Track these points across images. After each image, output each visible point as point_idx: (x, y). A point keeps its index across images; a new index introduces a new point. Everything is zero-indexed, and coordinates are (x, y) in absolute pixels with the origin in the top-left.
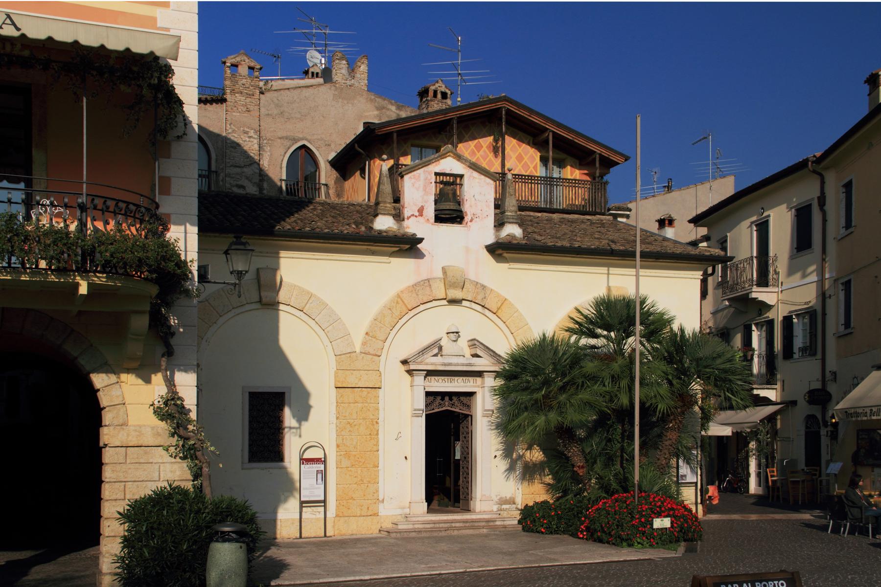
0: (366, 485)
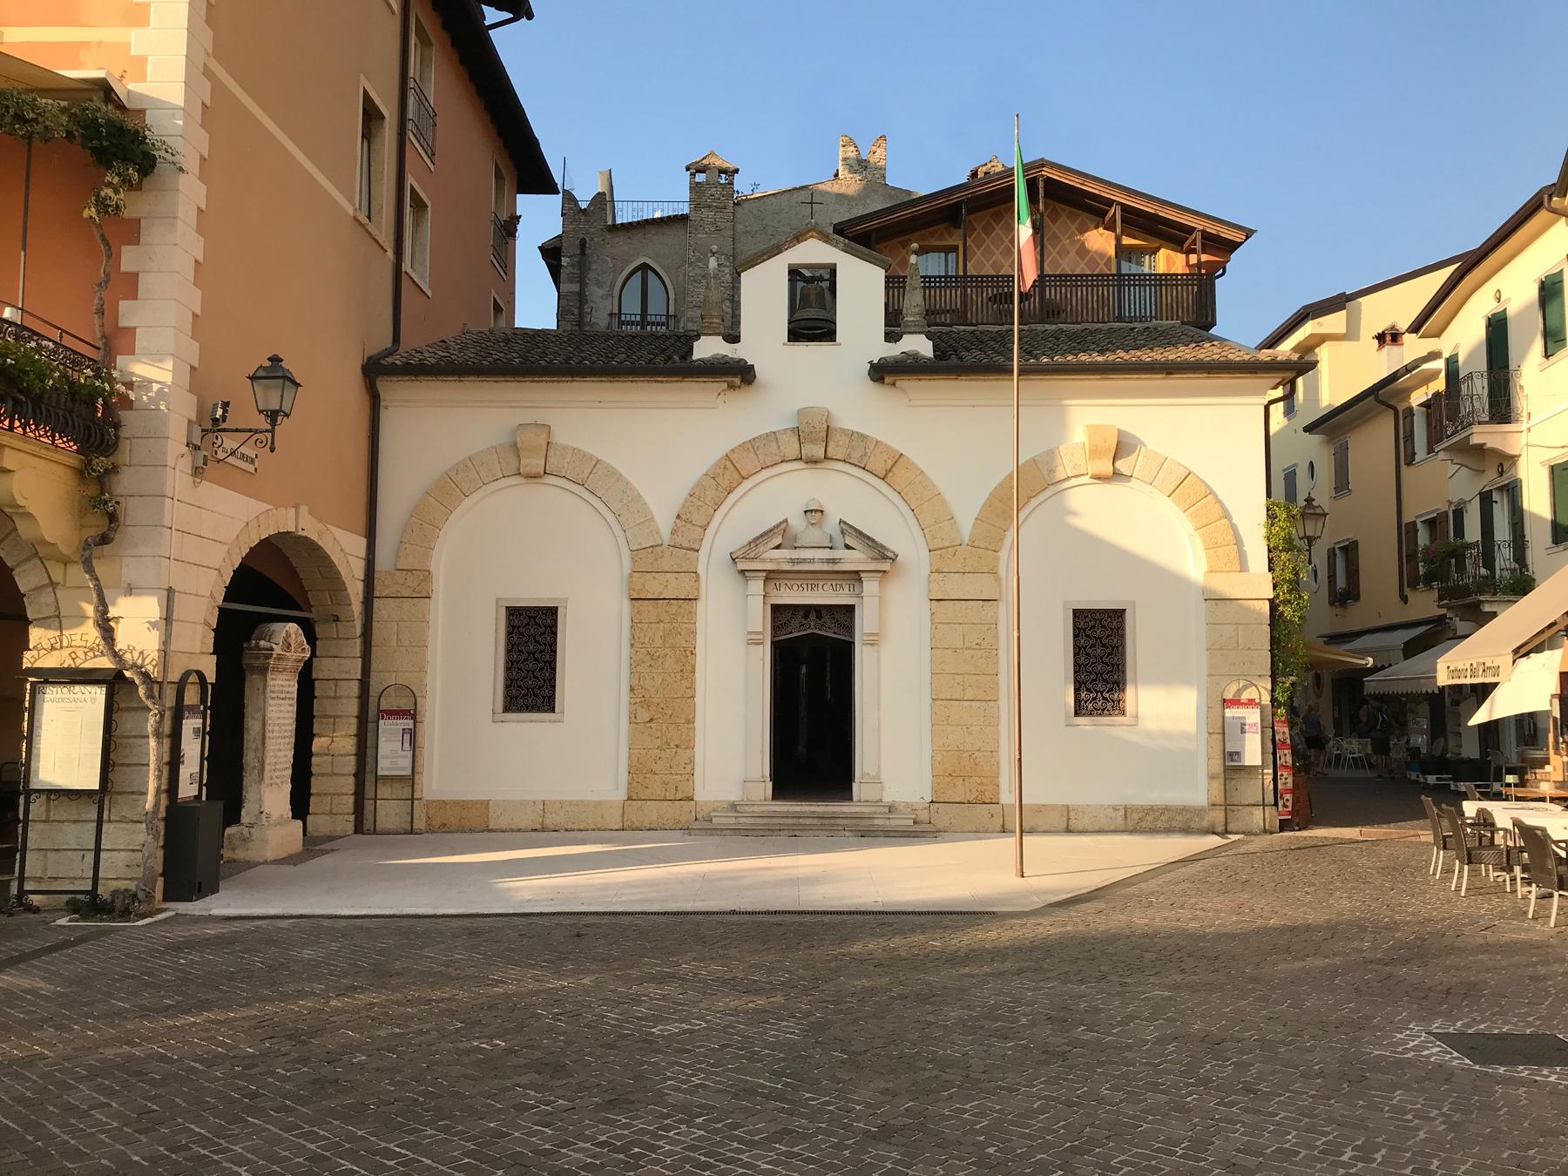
0: (674, 751)
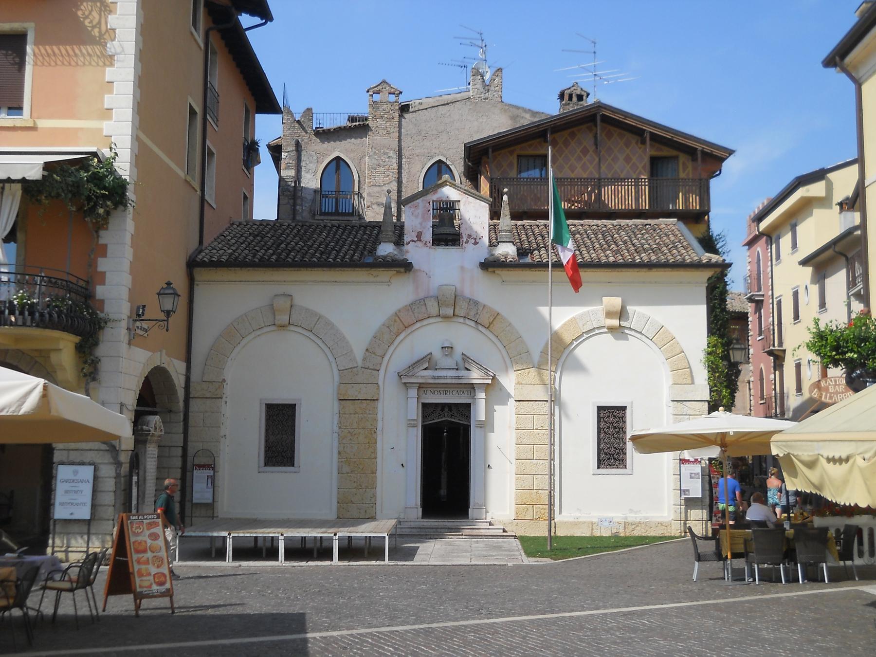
0: (364, 490)
